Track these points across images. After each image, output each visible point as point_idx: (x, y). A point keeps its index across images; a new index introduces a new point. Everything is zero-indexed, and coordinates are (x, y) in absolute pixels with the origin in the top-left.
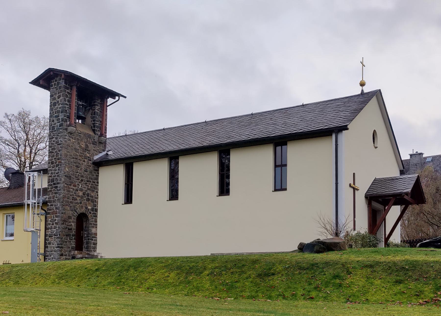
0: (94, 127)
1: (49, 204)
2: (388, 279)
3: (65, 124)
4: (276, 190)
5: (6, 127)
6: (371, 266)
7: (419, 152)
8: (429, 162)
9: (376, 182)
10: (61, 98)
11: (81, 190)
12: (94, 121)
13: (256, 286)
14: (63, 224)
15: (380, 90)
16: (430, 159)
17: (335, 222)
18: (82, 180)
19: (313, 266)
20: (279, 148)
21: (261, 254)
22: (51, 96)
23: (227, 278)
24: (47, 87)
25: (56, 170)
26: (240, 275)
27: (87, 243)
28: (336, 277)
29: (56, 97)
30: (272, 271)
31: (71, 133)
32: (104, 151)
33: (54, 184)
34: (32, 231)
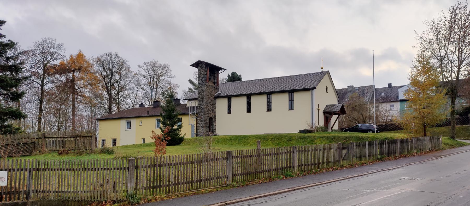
0: (214, 82)
1: (199, 114)
2: (327, 141)
3: (205, 82)
4: (289, 110)
5: (144, 69)
6: (322, 137)
7: (352, 85)
8: (357, 90)
9: (328, 106)
10: (203, 72)
11: (210, 108)
12: (214, 80)
13: (287, 144)
14: (204, 122)
15: (329, 71)
16: (357, 89)
17: (311, 123)
18: (211, 104)
19: (304, 138)
20: (290, 94)
21: (287, 134)
22: (199, 71)
23: (277, 141)
24: (197, 67)
25: (201, 101)
26: (281, 140)
27: (212, 129)
28: (311, 141)
29: (201, 72)
30: (292, 139)
31: (207, 86)
32: (218, 92)
33: (201, 106)
34: (192, 125)
